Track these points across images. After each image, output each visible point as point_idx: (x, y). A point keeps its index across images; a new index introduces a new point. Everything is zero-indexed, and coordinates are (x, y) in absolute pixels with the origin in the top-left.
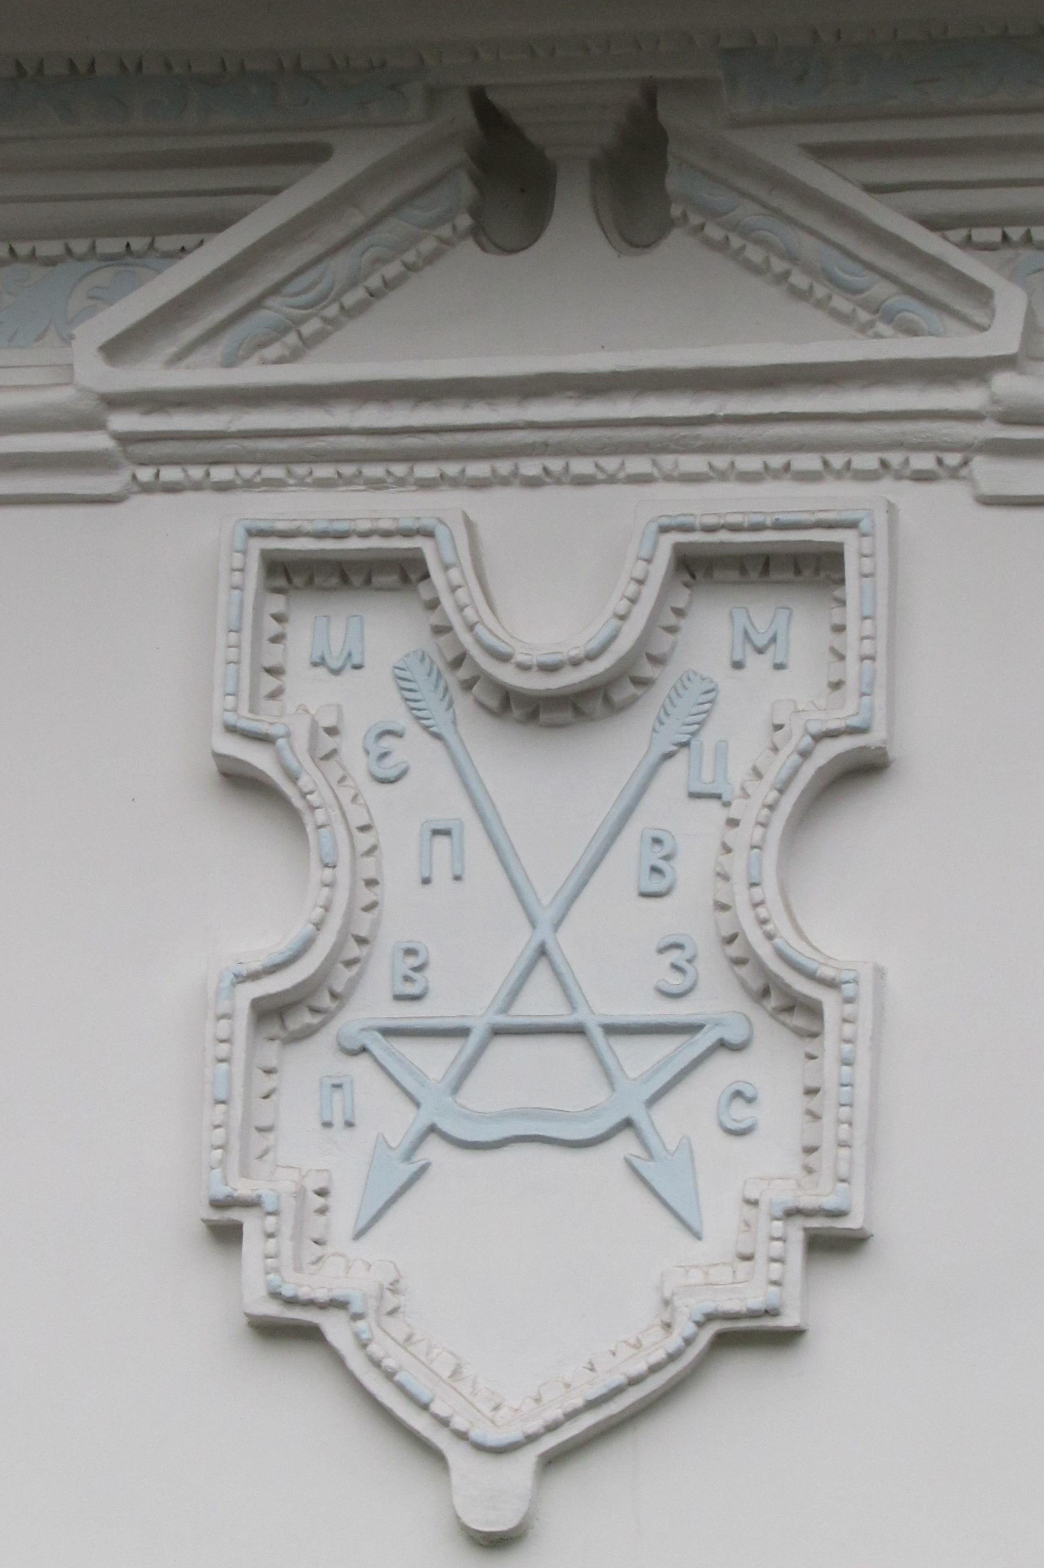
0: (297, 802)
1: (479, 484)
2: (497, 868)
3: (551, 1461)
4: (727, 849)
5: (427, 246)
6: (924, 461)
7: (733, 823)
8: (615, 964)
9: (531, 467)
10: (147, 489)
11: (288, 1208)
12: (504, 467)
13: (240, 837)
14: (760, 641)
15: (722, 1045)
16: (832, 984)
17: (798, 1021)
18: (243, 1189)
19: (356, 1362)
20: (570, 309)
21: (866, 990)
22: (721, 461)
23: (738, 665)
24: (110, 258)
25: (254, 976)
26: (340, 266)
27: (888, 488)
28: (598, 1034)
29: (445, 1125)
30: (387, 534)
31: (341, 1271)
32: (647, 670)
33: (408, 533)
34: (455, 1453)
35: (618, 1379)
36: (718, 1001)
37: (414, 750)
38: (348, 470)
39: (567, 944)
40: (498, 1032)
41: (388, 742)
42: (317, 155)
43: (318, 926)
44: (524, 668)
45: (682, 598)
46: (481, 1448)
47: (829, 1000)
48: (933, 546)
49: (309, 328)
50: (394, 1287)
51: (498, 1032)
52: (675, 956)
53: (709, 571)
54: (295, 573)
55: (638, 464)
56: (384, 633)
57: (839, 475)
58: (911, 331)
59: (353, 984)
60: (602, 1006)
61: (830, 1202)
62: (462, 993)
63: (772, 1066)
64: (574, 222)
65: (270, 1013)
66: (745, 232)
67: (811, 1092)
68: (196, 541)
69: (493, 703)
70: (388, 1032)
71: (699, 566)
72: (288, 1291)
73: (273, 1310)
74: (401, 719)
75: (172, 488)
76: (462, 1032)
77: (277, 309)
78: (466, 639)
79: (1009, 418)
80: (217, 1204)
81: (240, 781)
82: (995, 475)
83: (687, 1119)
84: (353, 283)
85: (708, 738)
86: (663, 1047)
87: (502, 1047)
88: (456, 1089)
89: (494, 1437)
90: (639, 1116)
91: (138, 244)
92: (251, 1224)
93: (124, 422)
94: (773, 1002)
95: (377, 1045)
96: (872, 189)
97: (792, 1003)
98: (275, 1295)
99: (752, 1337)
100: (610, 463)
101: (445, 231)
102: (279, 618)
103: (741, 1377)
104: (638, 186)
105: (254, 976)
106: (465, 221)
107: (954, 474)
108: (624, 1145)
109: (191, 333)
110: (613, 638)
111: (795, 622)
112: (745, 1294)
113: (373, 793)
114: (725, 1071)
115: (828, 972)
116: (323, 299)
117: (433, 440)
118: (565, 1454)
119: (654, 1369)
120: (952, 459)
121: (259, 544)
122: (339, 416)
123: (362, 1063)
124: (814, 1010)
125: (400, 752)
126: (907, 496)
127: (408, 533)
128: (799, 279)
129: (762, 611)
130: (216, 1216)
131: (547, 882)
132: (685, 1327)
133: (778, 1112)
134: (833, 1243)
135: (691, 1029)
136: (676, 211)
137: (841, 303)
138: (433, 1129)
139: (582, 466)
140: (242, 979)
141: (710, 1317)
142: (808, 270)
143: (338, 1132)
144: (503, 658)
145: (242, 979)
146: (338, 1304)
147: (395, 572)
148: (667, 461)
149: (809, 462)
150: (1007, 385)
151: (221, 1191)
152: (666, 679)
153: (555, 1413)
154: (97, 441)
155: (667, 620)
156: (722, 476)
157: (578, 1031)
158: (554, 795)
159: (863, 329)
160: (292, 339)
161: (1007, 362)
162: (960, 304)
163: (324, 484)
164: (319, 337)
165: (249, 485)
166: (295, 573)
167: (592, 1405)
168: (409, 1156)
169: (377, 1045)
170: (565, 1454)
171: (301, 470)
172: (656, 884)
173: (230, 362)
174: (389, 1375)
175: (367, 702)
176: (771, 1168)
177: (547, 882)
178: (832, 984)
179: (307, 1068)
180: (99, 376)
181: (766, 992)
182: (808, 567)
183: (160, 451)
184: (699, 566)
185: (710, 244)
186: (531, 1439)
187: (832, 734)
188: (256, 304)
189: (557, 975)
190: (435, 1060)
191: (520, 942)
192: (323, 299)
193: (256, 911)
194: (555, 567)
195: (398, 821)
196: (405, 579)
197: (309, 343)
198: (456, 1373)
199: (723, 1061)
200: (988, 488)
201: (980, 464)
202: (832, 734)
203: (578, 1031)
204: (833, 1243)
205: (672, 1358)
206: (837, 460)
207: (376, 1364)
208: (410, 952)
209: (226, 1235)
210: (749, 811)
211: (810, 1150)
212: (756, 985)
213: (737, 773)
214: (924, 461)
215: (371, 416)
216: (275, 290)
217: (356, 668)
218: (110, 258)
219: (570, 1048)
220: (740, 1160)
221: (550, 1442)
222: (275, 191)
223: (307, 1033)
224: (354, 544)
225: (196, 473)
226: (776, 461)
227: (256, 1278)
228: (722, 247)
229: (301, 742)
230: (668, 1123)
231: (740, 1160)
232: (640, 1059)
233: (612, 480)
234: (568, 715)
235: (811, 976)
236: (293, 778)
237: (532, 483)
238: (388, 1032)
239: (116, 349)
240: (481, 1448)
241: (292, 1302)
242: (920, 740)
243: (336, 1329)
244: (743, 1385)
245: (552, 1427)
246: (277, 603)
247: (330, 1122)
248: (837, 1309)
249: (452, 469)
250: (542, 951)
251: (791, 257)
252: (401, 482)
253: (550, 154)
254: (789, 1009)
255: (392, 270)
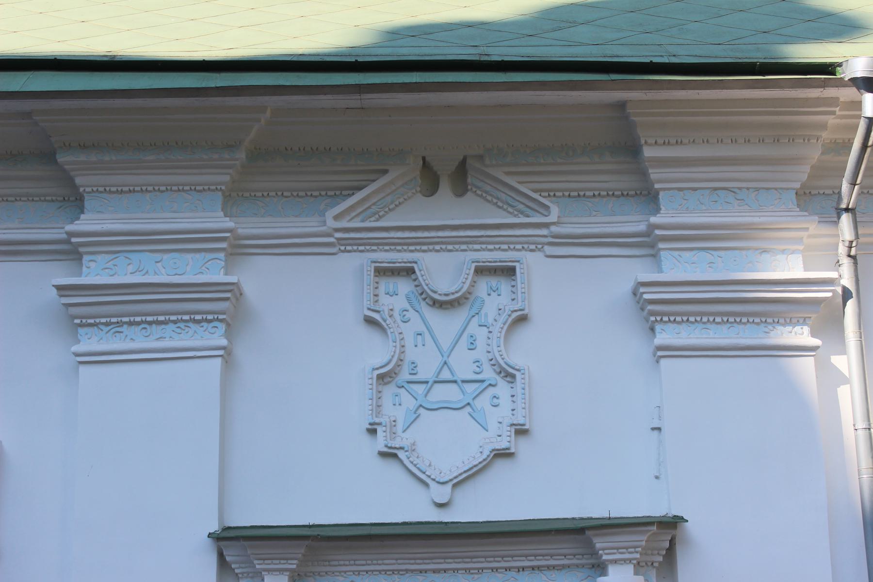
0: (386, 326)
1: (424, 251)
2: (434, 342)
3: (455, 486)
4: (489, 338)
5: (410, 194)
6: (533, 247)
7: (490, 332)
8: (463, 364)
9: (437, 247)
10: (343, 251)
11: (388, 426)
12: (431, 247)
13: (374, 336)
14: (494, 289)
15: (490, 385)
16: (518, 370)
17: (508, 379)
18: (377, 420)
19: (406, 462)
20: (446, 210)
21: (527, 372)
22: (484, 246)
23: (489, 295)
24: (331, 196)
25: (377, 369)
26: (389, 199)
27: (524, 252)
28: (460, 383)
29: (424, 405)
30: (405, 263)
31: (403, 439)
32: (468, 296)
33: (410, 262)
34: (432, 484)
35: (471, 466)
36: (488, 374)
37: (411, 314)
38: (393, 247)
39: (451, 361)
40: (435, 382)
41: (405, 313)
42: (385, 172)
43: (393, 357)
44: (440, 295)
45: (476, 279)
46: (438, 483)
47: (518, 374)
48: (534, 265)
49: (381, 214)
50: (414, 444)
51: (435, 382)
52: (477, 364)
53: (482, 272)
54: (381, 272)
55: (464, 247)
56: (404, 286)
57: (512, 250)
58: (528, 216)
59: (399, 371)
60: (461, 375)
61: (521, 422)
62: (426, 372)
63: (503, 389)
64: (445, 188)
65: (381, 378)
66: (486, 192)
67: (513, 396)
68: (351, 266)
69: (431, 303)
70: (409, 382)
71: (480, 271)
72: (389, 445)
73: (386, 450)
74: (408, 307)
75: (349, 251)
76: (427, 382)
77: (374, 209)
78: (426, 287)
79: (553, 237)
80: (370, 424)
81: (370, 322)
82: (549, 250)
83: (483, 402)
84: (392, 203)
85: (483, 312)
86: (477, 385)
87: (437, 386)
88: (426, 396)
89: (441, 481)
90: (471, 402)
91: (338, 193)
92: (380, 430)
93: (338, 235)
94: (502, 374)
95: (406, 385)
96: (519, 183)
97: (508, 375)
98: (386, 446)
99: (503, 454)
100: (457, 247)
101: (414, 191)
102: (377, 283)
103: (501, 464)
104: (461, 179)
105: (377, 369)
106: (419, 189)
107: (539, 250)
108: (468, 409)
109: (354, 214)
110: (462, 288)
111: (504, 285)
112: (503, 444)
113: (402, 325)
114: (491, 391)
115: (517, 367)
116: (385, 206)
117: (414, 240)
118: (458, 484)
119: (480, 463)
120: (540, 246)
121: (374, 265)
122: (392, 234)
123: (403, 389)
124: (513, 376)
125: (408, 315)
126: (529, 255)
127: (410, 262)
128: (500, 204)
129: (494, 281)
130: (370, 427)
131: (445, 345)
132: (486, 453)
133: (505, 402)
134: (521, 432)
135: (482, 381)
136: (469, 187)
137: (510, 209)
138: (421, 406)
139: (450, 247)
140: (374, 369)
141: (493, 450)
142: (502, 202)
143: (397, 407)
144: (435, 292)
145: (374, 369)
146: (402, 448)
147: (408, 272)
148: (471, 246)
149: (505, 247)
150: (553, 229)
151: (372, 421)
152: (472, 298)
153: (455, 474)
154: (332, 240)
155: (473, 283)
156: (484, 250)
157: (455, 382)
158: (446, 325)
159: (515, 216)
160: (377, 216)
161: (554, 224)
162: (541, 210)
163: (386, 251)
164: (384, 216)
165: (368, 251)
166: (381, 272)
167: (465, 472)
168: (415, 413)
169: (406, 385)
170: (458, 484)
171: (381, 247)
172: (472, 347)
173: (363, 221)
174: (415, 465)
175: (399, 303)
176: (504, 413)
177: (445, 345)
178: (518, 370)
179: (389, 391)
180: (331, 223)
181: (500, 372)
182: (509, 272)
183: (348, 243)
184: (480, 271)
185: (478, 195)
186: (451, 480)
187: (516, 311)
188: (369, 207)
189: (449, 369)
190: (420, 389)
191: (439, 360)
192: (385, 206)
193: (377, 352)
194: (443, 271)
195: (409, 331)
196: (408, 274)
197: (380, 217)
198: (430, 465)
199: (491, 388)
200: (548, 253)
201: (546, 248)
202: (516, 311)
203: (455, 382)
204: (521, 432)
205: (484, 460)
206: (512, 246)
207: (412, 463)
208: (413, 363)
209: (372, 432)
210: (496, 329)
211: (513, 410)
212: (498, 370)
213: (490, 320)
214: (533, 247)
215: (400, 234)
216: (374, 204)
217: (397, 296)
218: (331, 196)
219: (454, 386)
220: (499, 410)
221: (455, 481)
222: (374, 181)
223: (389, 382)
224: (398, 265)
225: (355, 248)
226: (497, 246)
227: (381, 442)
228: (481, 196)
229: (386, 312)
230: (478, 404)
231: (499, 410)
232: (470, 388)
233: (457, 250)
234: (449, 306)
235: (513, 368)
236: (385, 321)
237: (437, 251)
238: (409, 382)
239: (336, 218)
240: (438, 483)
241: (391, 448)
242: (536, 311)
243: (401, 454)
244: (501, 465)
245: (456, 477)
246: (377, 279)
247: (397, 406)
248: (523, 447)
249: (418, 247)
250: (445, 363)
251: (498, 199)
252: (405, 251)
253: (439, 173)
254: (506, 376)
255: (401, 200)
